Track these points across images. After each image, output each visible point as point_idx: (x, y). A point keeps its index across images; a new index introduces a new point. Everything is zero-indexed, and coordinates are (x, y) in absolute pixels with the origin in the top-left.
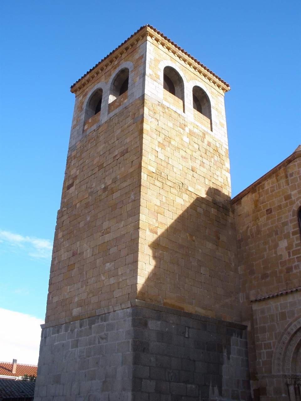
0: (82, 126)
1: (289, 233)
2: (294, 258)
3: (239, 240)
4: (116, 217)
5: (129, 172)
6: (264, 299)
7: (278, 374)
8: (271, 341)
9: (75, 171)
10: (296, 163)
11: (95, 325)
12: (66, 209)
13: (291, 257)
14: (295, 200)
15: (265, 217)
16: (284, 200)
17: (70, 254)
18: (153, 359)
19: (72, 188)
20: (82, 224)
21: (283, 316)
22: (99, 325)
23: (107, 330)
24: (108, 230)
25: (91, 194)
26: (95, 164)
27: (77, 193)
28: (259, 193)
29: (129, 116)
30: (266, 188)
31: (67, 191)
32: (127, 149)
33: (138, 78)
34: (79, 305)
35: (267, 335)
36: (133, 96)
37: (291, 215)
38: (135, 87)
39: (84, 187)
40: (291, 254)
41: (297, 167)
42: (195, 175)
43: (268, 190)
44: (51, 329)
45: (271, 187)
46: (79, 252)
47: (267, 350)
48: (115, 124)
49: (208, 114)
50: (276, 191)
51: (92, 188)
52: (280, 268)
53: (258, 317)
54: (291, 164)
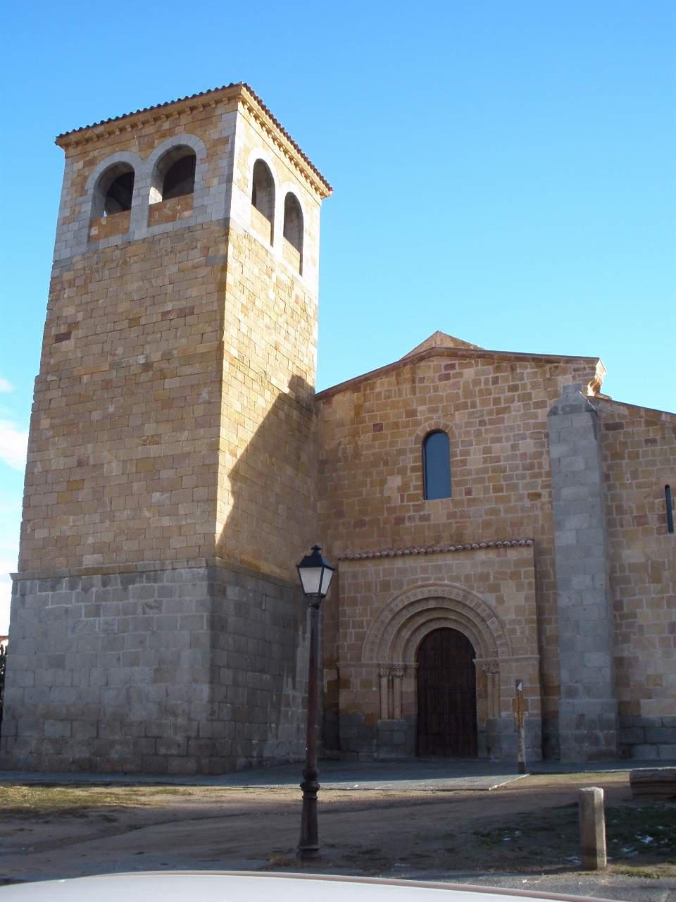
1: (406, 467)
2: (409, 505)
3: (322, 461)
4: (173, 421)
5: (197, 352)
6: (361, 559)
7: (371, 662)
8: (365, 619)
10: (432, 364)
11: (136, 585)
12: (55, 378)
13: (405, 503)
14: (423, 420)
15: (370, 434)
18: (231, 641)
20: (96, 416)
21: (386, 586)
22: (144, 587)
25: (114, 366)
26: (122, 313)
27: (80, 356)
28: (364, 395)
29: (196, 247)
30: (377, 390)
33: (215, 181)
34: (96, 549)
35: (359, 609)
39: (96, 349)
40: (405, 498)
41: (432, 370)
42: (279, 356)
44: (37, 582)
47: (357, 630)
49: (299, 245)
50: (394, 399)
52: (386, 515)
53: (346, 582)
54: (423, 363)
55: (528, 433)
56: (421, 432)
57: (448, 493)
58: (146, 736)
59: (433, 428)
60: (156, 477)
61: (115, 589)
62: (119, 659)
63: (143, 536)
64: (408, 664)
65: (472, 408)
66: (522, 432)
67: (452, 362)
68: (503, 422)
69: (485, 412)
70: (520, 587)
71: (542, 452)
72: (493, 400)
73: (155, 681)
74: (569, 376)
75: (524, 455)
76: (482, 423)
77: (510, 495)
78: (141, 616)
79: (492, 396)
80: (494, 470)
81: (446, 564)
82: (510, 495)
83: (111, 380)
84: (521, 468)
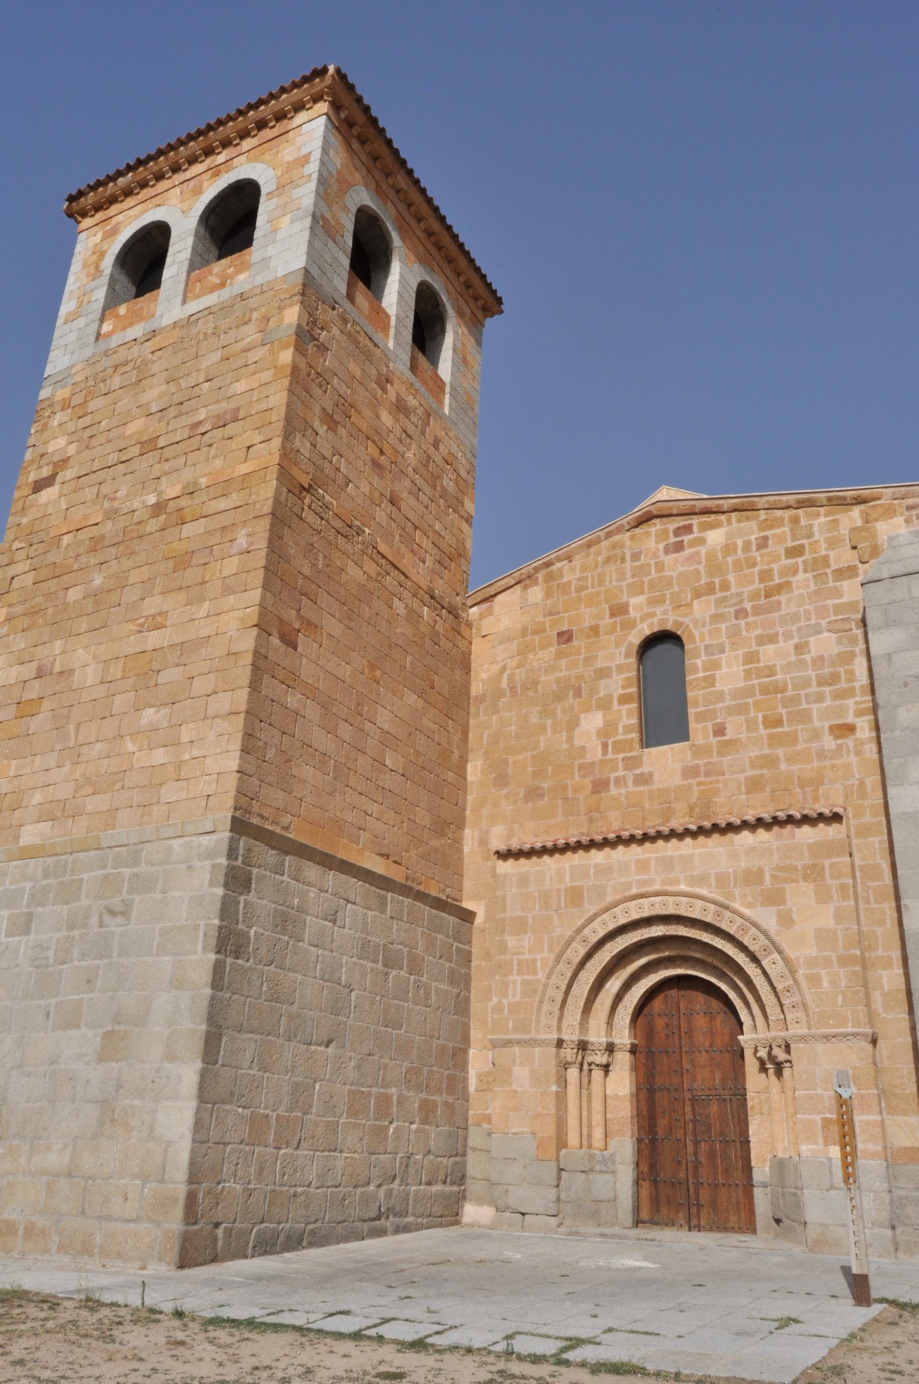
0: (94, 321)
2: (616, 759)
9: (64, 443)
10: (653, 530)
12: (23, 545)
13: (610, 756)
15: (553, 649)
16: (608, 616)
17: (30, 670)
19: (49, 490)
23: (131, 891)
24: (159, 619)
27: (64, 507)
31: (30, 497)
32: (237, 410)
36: (269, 268)
37: (620, 654)
38: (274, 242)
39: (89, 494)
41: (653, 538)
43: (570, 586)
45: (579, 579)
46: (57, 668)
47: (525, 977)
48: (205, 334)
50: (590, 590)
51: (115, 499)
55: (824, 623)
56: (635, 638)
57: (683, 735)
58: (70, 1175)
59: (656, 630)
60: (152, 683)
61: (61, 883)
62: (48, 1015)
63: (119, 785)
64: (616, 1041)
65: (721, 591)
66: (813, 622)
67: (687, 523)
68: (780, 610)
69: (745, 596)
70: (823, 896)
71: (853, 652)
72: (759, 575)
73: (102, 1058)
74: (899, 520)
75: (819, 661)
76: (740, 613)
77: (796, 730)
78: (96, 930)
79: (757, 569)
80: (765, 690)
81: (681, 856)
82: (796, 730)
83: (103, 537)
84: (814, 682)
